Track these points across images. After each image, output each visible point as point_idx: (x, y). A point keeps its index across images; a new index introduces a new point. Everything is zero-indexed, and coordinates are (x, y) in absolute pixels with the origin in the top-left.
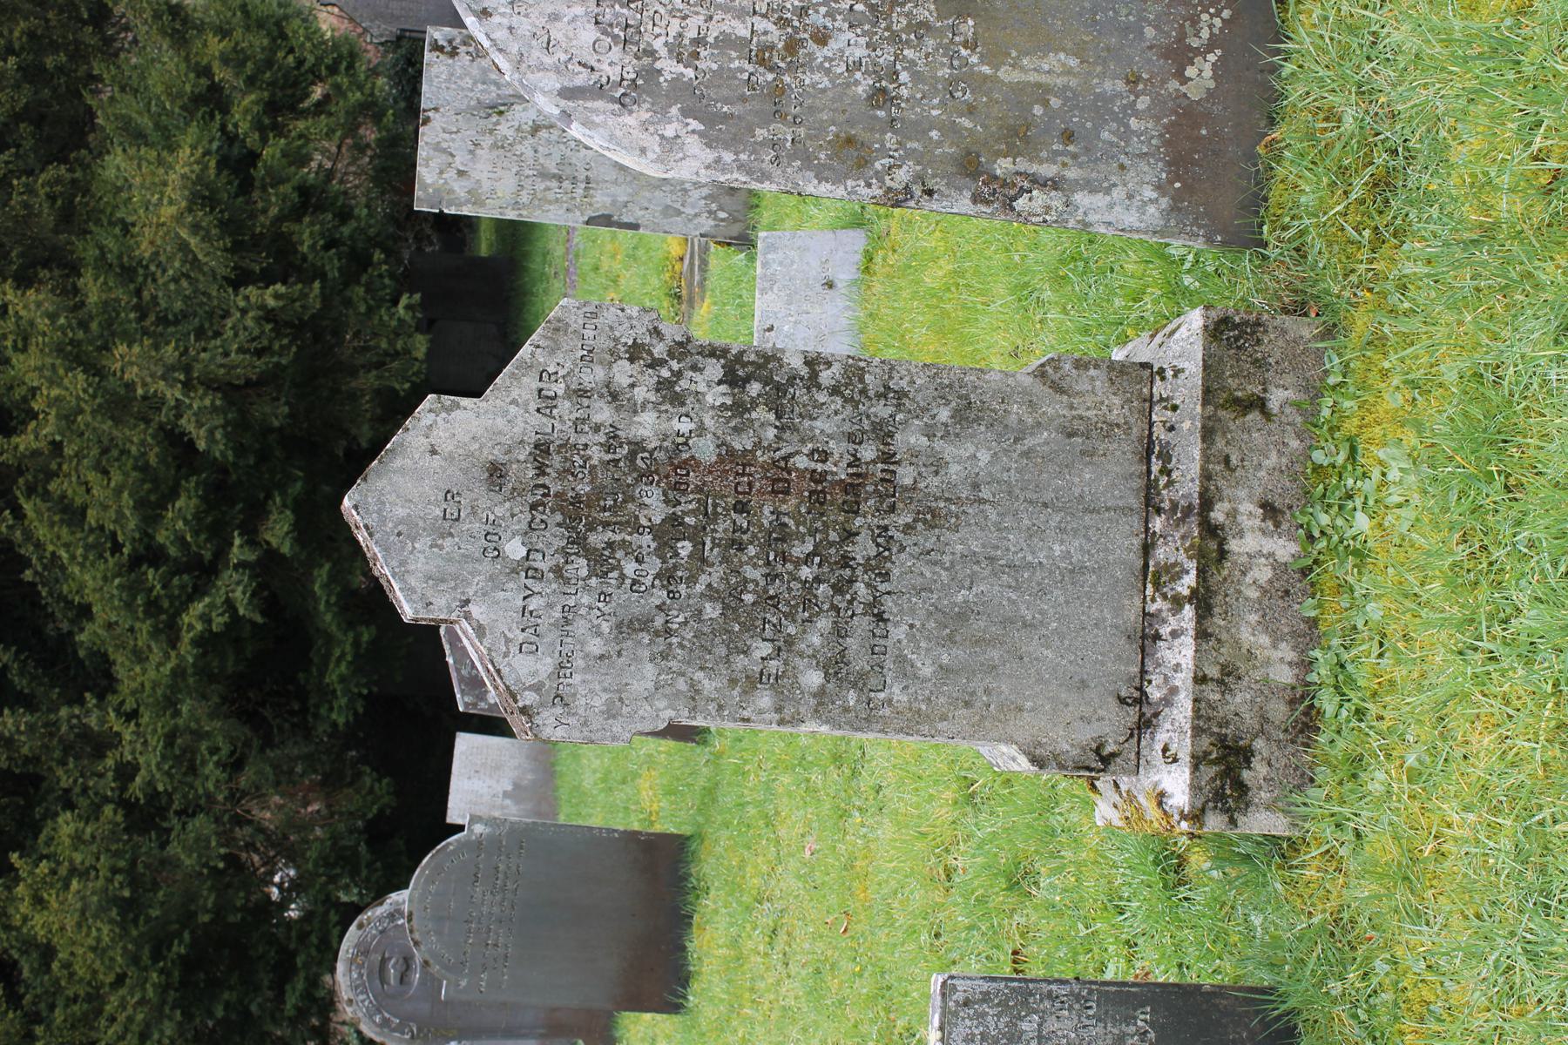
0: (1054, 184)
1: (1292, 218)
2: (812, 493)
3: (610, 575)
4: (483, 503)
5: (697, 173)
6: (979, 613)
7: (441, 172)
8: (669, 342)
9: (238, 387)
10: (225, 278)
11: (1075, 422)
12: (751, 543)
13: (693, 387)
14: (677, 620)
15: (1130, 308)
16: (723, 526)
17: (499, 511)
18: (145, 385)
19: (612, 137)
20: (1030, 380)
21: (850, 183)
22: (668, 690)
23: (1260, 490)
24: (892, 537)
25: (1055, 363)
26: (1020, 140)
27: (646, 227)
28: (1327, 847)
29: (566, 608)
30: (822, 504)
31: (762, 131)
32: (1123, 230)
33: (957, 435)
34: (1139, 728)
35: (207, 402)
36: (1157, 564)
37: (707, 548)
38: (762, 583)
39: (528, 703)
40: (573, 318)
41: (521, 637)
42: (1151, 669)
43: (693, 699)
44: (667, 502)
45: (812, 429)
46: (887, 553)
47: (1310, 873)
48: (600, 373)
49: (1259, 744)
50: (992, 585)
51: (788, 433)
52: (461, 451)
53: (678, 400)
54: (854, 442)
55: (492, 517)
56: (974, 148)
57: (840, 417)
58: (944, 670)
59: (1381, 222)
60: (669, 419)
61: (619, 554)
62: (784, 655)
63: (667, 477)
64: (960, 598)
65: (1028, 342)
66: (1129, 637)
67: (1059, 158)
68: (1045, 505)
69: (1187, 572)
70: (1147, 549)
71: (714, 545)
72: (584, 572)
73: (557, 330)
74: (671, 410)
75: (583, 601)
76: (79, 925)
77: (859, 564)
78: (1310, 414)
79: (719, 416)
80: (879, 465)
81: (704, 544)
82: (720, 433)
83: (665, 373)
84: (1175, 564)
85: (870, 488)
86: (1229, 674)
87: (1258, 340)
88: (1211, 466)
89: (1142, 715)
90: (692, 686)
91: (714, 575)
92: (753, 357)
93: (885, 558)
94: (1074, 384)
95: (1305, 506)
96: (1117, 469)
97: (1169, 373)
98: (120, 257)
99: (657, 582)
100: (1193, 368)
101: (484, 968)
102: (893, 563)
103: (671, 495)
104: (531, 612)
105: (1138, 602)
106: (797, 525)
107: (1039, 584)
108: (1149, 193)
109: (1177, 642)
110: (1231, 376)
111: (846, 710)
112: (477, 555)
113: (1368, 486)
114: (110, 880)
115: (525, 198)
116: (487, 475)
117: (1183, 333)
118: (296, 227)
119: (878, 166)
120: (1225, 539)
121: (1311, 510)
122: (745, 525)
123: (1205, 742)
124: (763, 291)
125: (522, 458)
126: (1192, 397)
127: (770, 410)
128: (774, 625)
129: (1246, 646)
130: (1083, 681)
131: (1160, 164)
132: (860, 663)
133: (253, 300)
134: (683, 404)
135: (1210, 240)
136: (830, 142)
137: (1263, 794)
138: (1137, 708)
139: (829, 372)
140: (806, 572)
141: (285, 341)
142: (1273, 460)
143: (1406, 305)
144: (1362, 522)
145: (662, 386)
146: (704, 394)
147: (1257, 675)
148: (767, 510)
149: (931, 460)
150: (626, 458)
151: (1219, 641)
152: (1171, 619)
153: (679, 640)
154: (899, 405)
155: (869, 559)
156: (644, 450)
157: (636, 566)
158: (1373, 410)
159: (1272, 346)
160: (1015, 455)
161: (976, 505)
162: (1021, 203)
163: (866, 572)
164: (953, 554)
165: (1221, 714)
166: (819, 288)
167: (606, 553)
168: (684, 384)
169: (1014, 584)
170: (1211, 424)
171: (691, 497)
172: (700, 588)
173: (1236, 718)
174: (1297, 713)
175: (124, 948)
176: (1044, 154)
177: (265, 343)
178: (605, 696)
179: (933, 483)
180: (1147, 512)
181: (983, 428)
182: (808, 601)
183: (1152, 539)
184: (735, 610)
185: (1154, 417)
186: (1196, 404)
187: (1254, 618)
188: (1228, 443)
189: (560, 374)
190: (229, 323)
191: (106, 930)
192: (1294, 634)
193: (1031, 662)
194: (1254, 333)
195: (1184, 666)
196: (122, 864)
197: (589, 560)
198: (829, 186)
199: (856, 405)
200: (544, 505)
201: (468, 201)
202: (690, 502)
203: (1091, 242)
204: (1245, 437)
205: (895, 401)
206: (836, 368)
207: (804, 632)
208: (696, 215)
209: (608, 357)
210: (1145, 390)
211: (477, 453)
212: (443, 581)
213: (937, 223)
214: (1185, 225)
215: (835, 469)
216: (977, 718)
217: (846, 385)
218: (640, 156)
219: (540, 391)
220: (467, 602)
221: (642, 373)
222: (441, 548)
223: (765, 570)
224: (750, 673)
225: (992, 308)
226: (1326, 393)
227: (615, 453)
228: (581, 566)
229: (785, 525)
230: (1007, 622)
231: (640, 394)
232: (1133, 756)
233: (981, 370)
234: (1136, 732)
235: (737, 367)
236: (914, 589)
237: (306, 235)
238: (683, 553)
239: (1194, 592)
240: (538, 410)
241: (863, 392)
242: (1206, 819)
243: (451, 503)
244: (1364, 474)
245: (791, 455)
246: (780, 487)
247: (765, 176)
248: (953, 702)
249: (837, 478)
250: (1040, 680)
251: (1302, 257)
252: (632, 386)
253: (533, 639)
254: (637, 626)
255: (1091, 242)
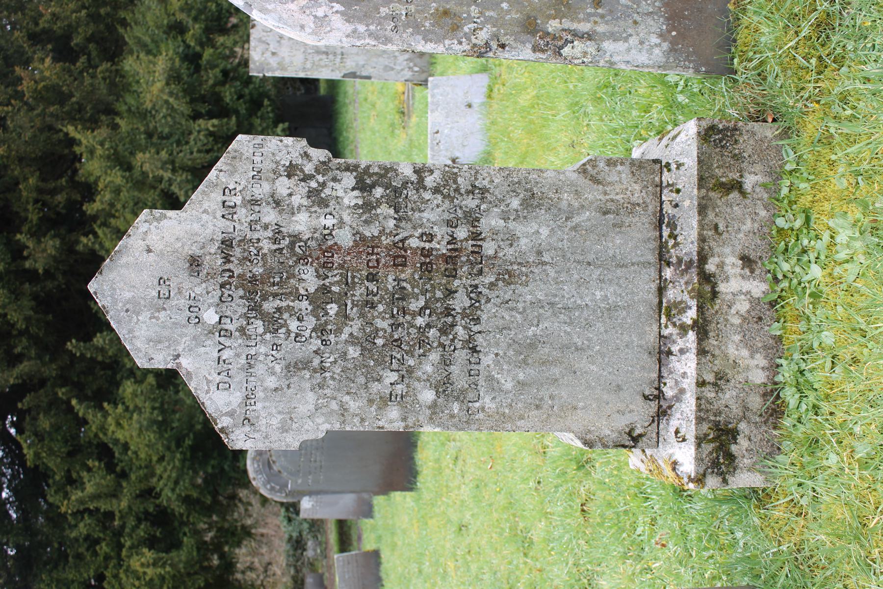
0: (589, 36)
1: (755, 53)
2: (422, 264)
3: (280, 331)
4: (186, 285)
5: (341, 41)
6: (544, 343)
7: (263, 54)
8: (315, 162)
9: (199, 169)
10: (189, 116)
11: (608, 204)
12: (380, 302)
13: (334, 193)
14: (329, 360)
15: (643, 117)
16: (359, 292)
17: (198, 290)
18: (153, 171)
19: (280, 19)
20: (576, 175)
21: (447, 42)
22: (324, 410)
23: (740, 247)
24: (480, 293)
25: (593, 162)
26: (564, 6)
27: (375, 78)
28: (791, 497)
29: (249, 357)
30: (430, 272)
31: (385, 9)
32: (637, 66)
33: (525, 217)
34: (658, 416)
35: (184, 176)
36: (669, 301)
37: (349, 308)
38: (389, 330)
39: (225, 425)
40: (246, 149)
41: (218, 379)
42: (666, 375)
43: (343, 415)
44: (318, 276)
45: (421, 218)
46: (477, 304)
47: (776, 514)
48: (266, 187)
49: (742, 426)
50: (553, 322)
51: (404, 222)
52: (169, 249)
53: (323, 203)
54: (451, 226)
55: (193, 295)
56: (533, 14)
57: (441, 209)
58: (521, 384)
59: (824, 52)
60: (318, 217)
61: (286, 316)
62: (406, 380)
63: (318, 259)
64: (530, 333)
65: (579, 139)
66: (650, 353)
67: (592, 18)
68: (589, 264)
69: (690, 308)
70: (661, 291)
71: (354, 306)
72: (261, 330)
73: (234, 158)
74: (319, 210)
75: (261, 350)
76: (139, 435)
77: (458, 313)
78: (773, 190)
79: (354, 213)
80: (470, 242)
81: (346, 305)
82: (354, 225)
83: (314, 184)
84: (681, 302)
85: (464, 259)
86: (720, 379)
87: (736, 141)
88: (705, 232)
89: (660, 407)
90: (342, 406)
91: (355, 327)
92: (376, 170)
93: (476, 307)
94: (606, 177)
95: (771, 257)
96: (639, 235)
97: (673, 167)
98: (138, 108)
99: (314, 334)
100: (691, 162)
101: (310, 473)
102: (482, 311)
103: (321, 271)
104: (224, 361)
105: (655, 328)
106: (413, 288)
107: (586, 320)
108: (654, 40)
109: (683, 357)
110: (717, 167)
111: (452, 416)
112: (183, 322)
113: (820, 245)
114: (152, 413)
115: (308, 65)
116: (188, 264)
117: (682, 137)
118: (222, 89)
119: (466, 29)
120: (716, 283)
121: (776, 260)
122: (375, 290)
123: (705, 427)
124: (432, 111)
125: (213, 251)
126: (690, 183)
127: (390, 206)
128: (399, 360)
129: (732, 358)
130: (618, 386)
131: (662, 20)
132: (461, 382)
133: (203, 126)
134: (327, 206)
135: (697, 71)
136: (432, 14)
137: (745, 460)
138: (657, 402)
139: (432, 177)
140: (420, 321)
141: (220, 145)
142: (748, 225)
143: (849, 112)
144: (816, 271)
145: (313, 193)
146: (342, 198)
147: (740, 378)
148: (390, 279)
149: (507, 236)
150: (287, 247)
151: (713, 356)
152: (679, 341)
153: (331, 374)
154: (483, 198)
155: (465, 309)
156: (301, 240)
157: (298, 323)
158: (823, 190)
159: (746, 145)
160: (567, 230)
161: (540, 266)
162: (566, 51)
163: (463, 318)
164: (525, 302)
165: (716, 407)
166: (463, 108)
167: (276, 315)
168: (327, 191)
169: (568, 321)
170: (704, 202)
171: (336, 272)
172: (344, 336)
173: (726, 409)
174: (768, 403)
175: (163, 443)
176: (581, 16)
177: (210, 147)
178: (280, 417)
179: (509, 252)
180: (661, 265)
181: (543, 212)
182: (422, 342)
183: (665, 284)
184: (370, 351)
185: (664, 198)
186: (693, 188)
187: (737, 338)
188: (716, 215)
189: (238, 189)
190: (192, 137)
191: (152, 436)
192: (766, 347)
193: (582, 375)
194: (733, 135)
195: (689, 374)
196: (157, 405)
197: (264, 321)
198: (432, 45)
199: (452, 200)
200: (230, 284)
201: (278, 69)
202: (335, 276)
203: (616, 75)
204: (729, 210)
205: (479, 196)
206: (437, 175)
207: (420, 363)
208: (402, 70)
209: (272, 175)
210: (657, 179)
211: (180, 250)
212: (160, 342)
213: (526, 67)
214: (680, 61)
215: (438, 246)
216: (545, 416)
217: (444, 186)
218: (300, 31)
219: (224, 202)
220: (178, 356)
221: (297, 185)
222: (157, 318)
223: (391, 321)
224: (382, 394)
225: (557, 118)
226: (784, 176)
227: (279, 244)
228: (259, 326)
229: (404, 288)
230: (564, 348)
231: (296, 200)
232: (654, 435)
233: (541, 170)
234: (656, 419)
235: (366, 177)
236: (498, 328)
237: (228, 94)
238: (332, 312)
239: (695, 322)
240: (223, 216)
241: (457, 190)
242: (707, 481)
243: (164, 286)
244: (817, 236)
245: (406, 238)
246: (399, 261)
247: (387, 40)
248: (528, 406)
249: (440, 253)
250: (589, 387)
251: (763, 80)
252: (290, 195)
253: (227, 379)
254: (301, 366)
255: (616, 75)
